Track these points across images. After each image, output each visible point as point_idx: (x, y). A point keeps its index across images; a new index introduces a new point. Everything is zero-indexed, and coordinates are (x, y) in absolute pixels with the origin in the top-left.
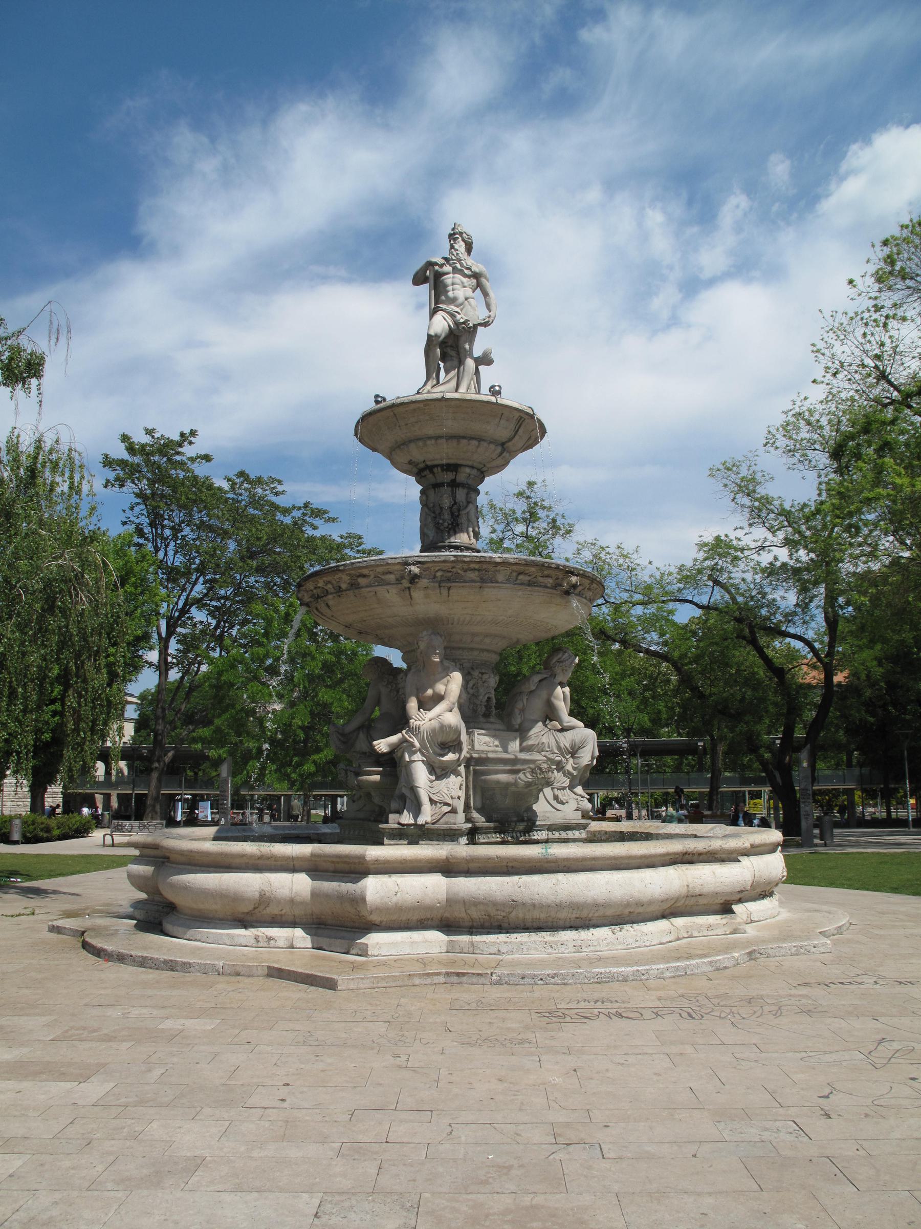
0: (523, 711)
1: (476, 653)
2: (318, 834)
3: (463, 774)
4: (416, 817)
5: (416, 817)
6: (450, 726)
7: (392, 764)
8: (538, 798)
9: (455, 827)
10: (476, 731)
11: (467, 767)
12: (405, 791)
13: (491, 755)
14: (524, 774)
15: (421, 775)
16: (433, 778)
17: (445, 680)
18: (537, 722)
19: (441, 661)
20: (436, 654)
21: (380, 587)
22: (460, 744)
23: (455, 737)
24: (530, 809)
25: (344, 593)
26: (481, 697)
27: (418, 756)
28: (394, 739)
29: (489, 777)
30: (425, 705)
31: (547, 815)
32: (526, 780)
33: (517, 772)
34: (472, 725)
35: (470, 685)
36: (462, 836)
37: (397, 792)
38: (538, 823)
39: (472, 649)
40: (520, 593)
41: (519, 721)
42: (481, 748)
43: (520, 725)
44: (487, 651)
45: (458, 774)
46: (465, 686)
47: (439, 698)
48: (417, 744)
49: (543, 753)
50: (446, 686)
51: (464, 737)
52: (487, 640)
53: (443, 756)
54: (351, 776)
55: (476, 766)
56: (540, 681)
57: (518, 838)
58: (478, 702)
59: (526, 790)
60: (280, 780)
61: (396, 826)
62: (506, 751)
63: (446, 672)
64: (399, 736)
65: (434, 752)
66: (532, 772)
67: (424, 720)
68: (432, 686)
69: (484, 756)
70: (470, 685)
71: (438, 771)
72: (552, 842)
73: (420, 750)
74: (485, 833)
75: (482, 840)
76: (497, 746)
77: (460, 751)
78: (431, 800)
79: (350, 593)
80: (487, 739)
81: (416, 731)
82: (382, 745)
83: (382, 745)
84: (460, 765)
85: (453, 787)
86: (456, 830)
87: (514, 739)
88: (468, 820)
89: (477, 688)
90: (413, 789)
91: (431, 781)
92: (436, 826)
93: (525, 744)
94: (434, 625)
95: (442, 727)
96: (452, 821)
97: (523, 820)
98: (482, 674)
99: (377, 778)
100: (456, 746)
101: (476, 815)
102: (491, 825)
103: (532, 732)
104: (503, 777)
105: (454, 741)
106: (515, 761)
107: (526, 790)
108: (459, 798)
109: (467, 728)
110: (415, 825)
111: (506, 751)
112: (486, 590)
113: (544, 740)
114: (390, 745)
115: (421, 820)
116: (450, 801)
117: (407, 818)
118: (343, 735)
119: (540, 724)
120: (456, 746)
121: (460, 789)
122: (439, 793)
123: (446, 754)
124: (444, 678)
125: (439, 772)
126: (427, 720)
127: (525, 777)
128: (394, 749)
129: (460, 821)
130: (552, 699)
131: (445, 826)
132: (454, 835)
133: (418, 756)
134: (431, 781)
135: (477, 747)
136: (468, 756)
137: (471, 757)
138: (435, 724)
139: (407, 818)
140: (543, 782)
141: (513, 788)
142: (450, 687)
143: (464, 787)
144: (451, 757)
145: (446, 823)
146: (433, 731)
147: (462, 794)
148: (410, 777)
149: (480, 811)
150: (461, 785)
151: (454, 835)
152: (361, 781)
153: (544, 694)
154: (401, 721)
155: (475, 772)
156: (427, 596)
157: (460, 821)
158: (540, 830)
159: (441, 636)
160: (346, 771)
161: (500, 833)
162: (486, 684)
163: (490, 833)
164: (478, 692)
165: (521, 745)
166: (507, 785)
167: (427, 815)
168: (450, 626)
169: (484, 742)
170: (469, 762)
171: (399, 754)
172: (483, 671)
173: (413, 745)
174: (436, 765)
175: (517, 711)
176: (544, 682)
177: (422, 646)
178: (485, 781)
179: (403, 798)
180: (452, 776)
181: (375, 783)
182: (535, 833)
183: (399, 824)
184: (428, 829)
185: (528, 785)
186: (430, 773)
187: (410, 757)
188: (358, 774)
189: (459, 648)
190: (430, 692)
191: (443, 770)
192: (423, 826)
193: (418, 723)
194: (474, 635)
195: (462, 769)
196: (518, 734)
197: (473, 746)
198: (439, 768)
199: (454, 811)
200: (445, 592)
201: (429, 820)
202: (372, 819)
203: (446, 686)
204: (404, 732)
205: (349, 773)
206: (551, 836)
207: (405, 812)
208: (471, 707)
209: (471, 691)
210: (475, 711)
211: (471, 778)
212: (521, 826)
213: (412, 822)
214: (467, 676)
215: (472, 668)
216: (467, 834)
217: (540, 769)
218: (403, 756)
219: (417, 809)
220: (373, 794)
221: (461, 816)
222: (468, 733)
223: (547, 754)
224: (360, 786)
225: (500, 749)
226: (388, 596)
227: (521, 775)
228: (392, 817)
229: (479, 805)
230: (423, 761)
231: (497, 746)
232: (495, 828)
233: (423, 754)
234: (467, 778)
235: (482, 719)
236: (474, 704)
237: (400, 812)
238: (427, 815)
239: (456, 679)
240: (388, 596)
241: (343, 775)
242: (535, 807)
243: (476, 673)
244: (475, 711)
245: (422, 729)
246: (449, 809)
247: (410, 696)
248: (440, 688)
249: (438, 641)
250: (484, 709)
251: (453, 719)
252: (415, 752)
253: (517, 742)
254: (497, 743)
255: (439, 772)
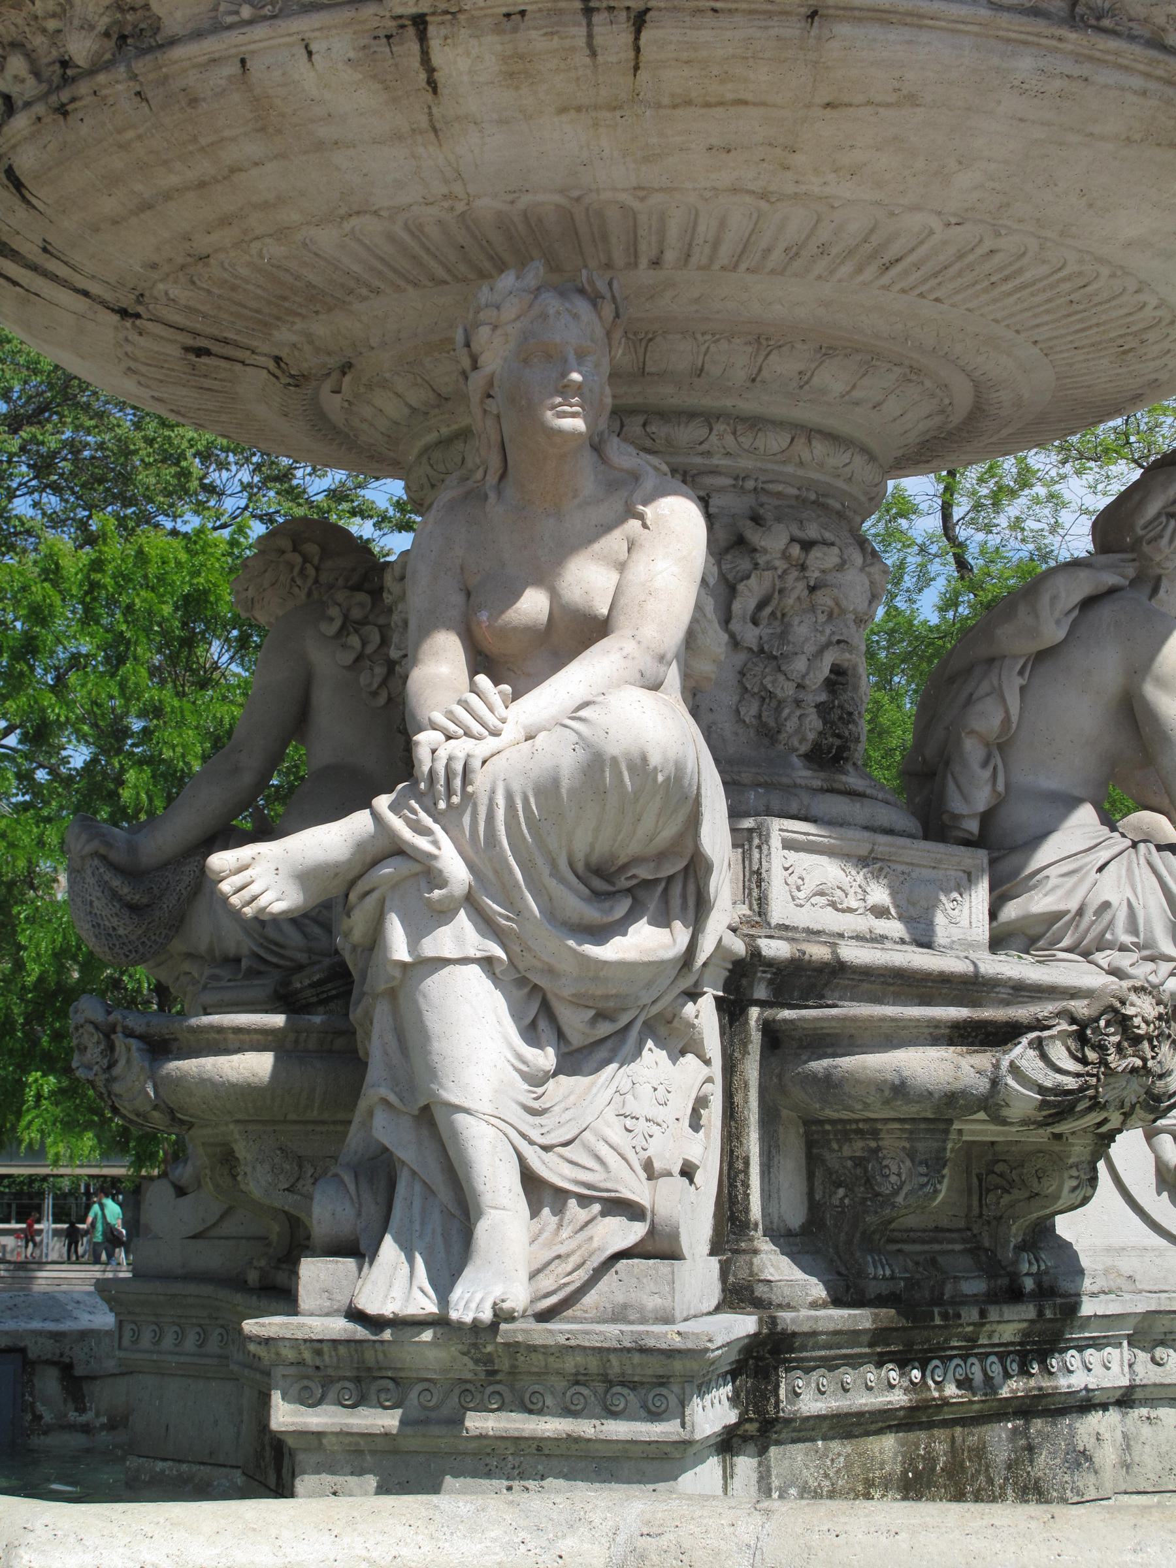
0: (1001, 747)
1: (775, 441)
2: (57, 1336)
3: (713, 1044)
4: (444, 1280)
5: (444, 1280)
6: (640, 766)
7: (324, 977)
8: (1093, 1181)
9: (667, 1336)
10: (778, 828)
11: (731, 1010)
12: (389, 1131)
13: (854, 954)
14: (1039, 1046)
15: (474, 1039)
16: (546, 1058)
17: (615, 541)
18: (1071, 803)
19: (596, 445)
20: (566, 390)
21: (260, 31)
22: (696, 869)
23: (670, 831)
24: (1042, 1235)
25: (83, 88)
26: (799, 665)
27: (459, 936)
28: (329, 841)
29: (848, 1063)
30: (510, 662)
31: (1127, 1265)
32: (1050, 1079)
33: (1001, 1035)
34: (751, 798)
35: (745, 603)
36: (703, 1388)
37: (355, 1137)
38: (1088, 1308)
39: (756, 423)
40: (1025, 64)
41: (982, 799)
42: (803, 918)
43: (986, 818)
44: (832, 437)
45: (682, 1044)
46: (723, 584)
47: (580, 631)
48: (455, 868)
49: (1102, 958)
50: (621, 567)
51: (715, 836)
52: (832, 378)
53: (600, 933)
54: (130, 1053)
55: (779, 1004)
56: (1088, 603)
57: (990, 1384)
58: (786, 690)
59: (1041, 1136)
60: (71, 1127)
61: (339, 1327)
62: (925, 941)
63: (624, 500)
64: (358, 823)
65: (551, 913)
66: (1081, 1038)
67: (488, 734)
68: (544, 574)
69: (818, 952)
70: (745, 603)
71: (575, 1021)
72: (1152, 1402)
73: (470, 900)
74: (830, 1365)
75: (811, 1404)
76: (880, 912)
77: (698, 909)
78: (531, 1183)
79: (116, 84)
80: (828, 871)
81: (449, 796)
82: (262, 876)
83: (262, 876)
84: (693, 995)
85: (661, 1115)
86: (671, 1354)
87: (967, 881)
88: (738, 1294)
89: (780, 617)
90: (432, 1120)
91: (536, 1079)
92: (559, 1330)
93: (1011, 911)
94: (565, 249)
95: (596, 765)
96: (652, 1303)
97: (1015, 1295)
98: (807, 545)
99: (256, 1065)
100: (677, 887)
101: (776, 1267)
102: (861, 1318)
103: (1046, 853)
104: (932, 1066)
105: (661, 857)
106: (969, 988)
107: (1041, 1136)
108: (688, 1172)
109: (735, 813)
110: (440, 1322)
111: (925, 941)
112: (843, 29)
113: (1111, 888)
114: (306, 877)
115: (471, 1301)
116: (636, 1189)
117: (394, 1283)
118: (132, 873)
119: (1086, 814)
120: (677, 887)
121: (695, 1124)
122: (578, 1153)
123: (620, 927)
124: (607, 528)
125: (580, 1027)
126: (511, 732)
127: (1040, 1066)
128: (334, 901)
129: (691, 1306)
130: (1151, 691)
131: (612, 1333)
132: (662, 1381)
133: (459, 936)
134: (536, 1079)
135: (780, 910)
136: (739, 947)
137: (755, 954)
138: (559, 754)
139: (394, 1283)
140: (1133, 1091)
141: (976, 1128)
142: (639, 569)
143: (714, 1114)
144: (645, 942)
145: (619, 1315)
146: (547, 789)
147: (705, 1150)
148: (412, 1043)
149: (800, 1243)
150: (701, 1102)
151: (662, 1381)
152: (180, 1081)
153: (1104, 666)
154: (383, 755)
155: (773, 1036)
156: (517, 70)
157: (691, 1306)
158: (1097, 1344)
159: (595, 300)
160: (108, 1033)
161: (903, 1364)
162: (824, 599)
163: (854, 1362)
164: (783, 636)
165: (993, 915)
166: (953, 1103)
167: (507, 1269)
168: (644, 275)
169: (817, 891)
170: (744, 982)
171: (358, 923)
172: (812, 531)
173: (430, 875)
174: (561, 991)
175: (972, 749)
176: (1106, 612)
177: (495, 354)
178: (829, 1084)
179: (380, 1172)
180: (653, 1057)
181: (245, 1092)
182: (1072, 1357)
183: (356, 1315)
184: (513, 1347)
185: (1059, 1106)
186: (531, 1033)
187: (414, 942)
188: (161, 1048)
189: (692, 415)
190: (533, 605)
191: (602, 1016)
192: (479, 1333)
193: (460, 748)
194: (764, 340)
195: (704, 1014)
196: (982, 856)
197: (761, 904)
198: (579, 1002)
199: (660, 1247)
200: (614, 38)
201: (518, 1296)
202: (253, 1277)
203: (621, 567)
204: (382, 802)
205: (119, 1039)
206: (1146, 1373)
207: (389, 1248)
208: (750, 711)
209: (750, 635)
210: (768, 733)
211: (751, 1070)
212: (1010, 1323)
213: (425, 1304)
214: (730, 545)
215: (757, 520)
216: (734, 1374)
217: (1124, 1022)
218: (376, 938)
219: (451, 1240)
220: (242, 1150)
221: (699, 1275)
222: (743, 840)
223: (1124, 961)
224: (178, 1111)
225: (894, 928)
226: (305, 75)
227: (1022, 1053)
228: (316, 1275)
229: (794, 1215)
230: (487, 963)
231: (880, 912)
232: (879, 1336)
233: (487, 925)
234: (730, 1068)
235: (803, 774)
236: (766, 696)
237: (359, 1250)
238: (507, 1269)
239: (677, 529)
240: (305, 75)
241: (94, 1053)
242: (1066, 1226)
243: (773, 542)
244: (768, 733)
245: (481, 782)
246: (634, 1232)
247: (426, 631)
248: (589, 579)
249: (575, 325)
250: (814, 723)
251: (657, 727)
252: (442, 915)
253: (980, 895)
254: (880, 894)
255: (580, 1027)
